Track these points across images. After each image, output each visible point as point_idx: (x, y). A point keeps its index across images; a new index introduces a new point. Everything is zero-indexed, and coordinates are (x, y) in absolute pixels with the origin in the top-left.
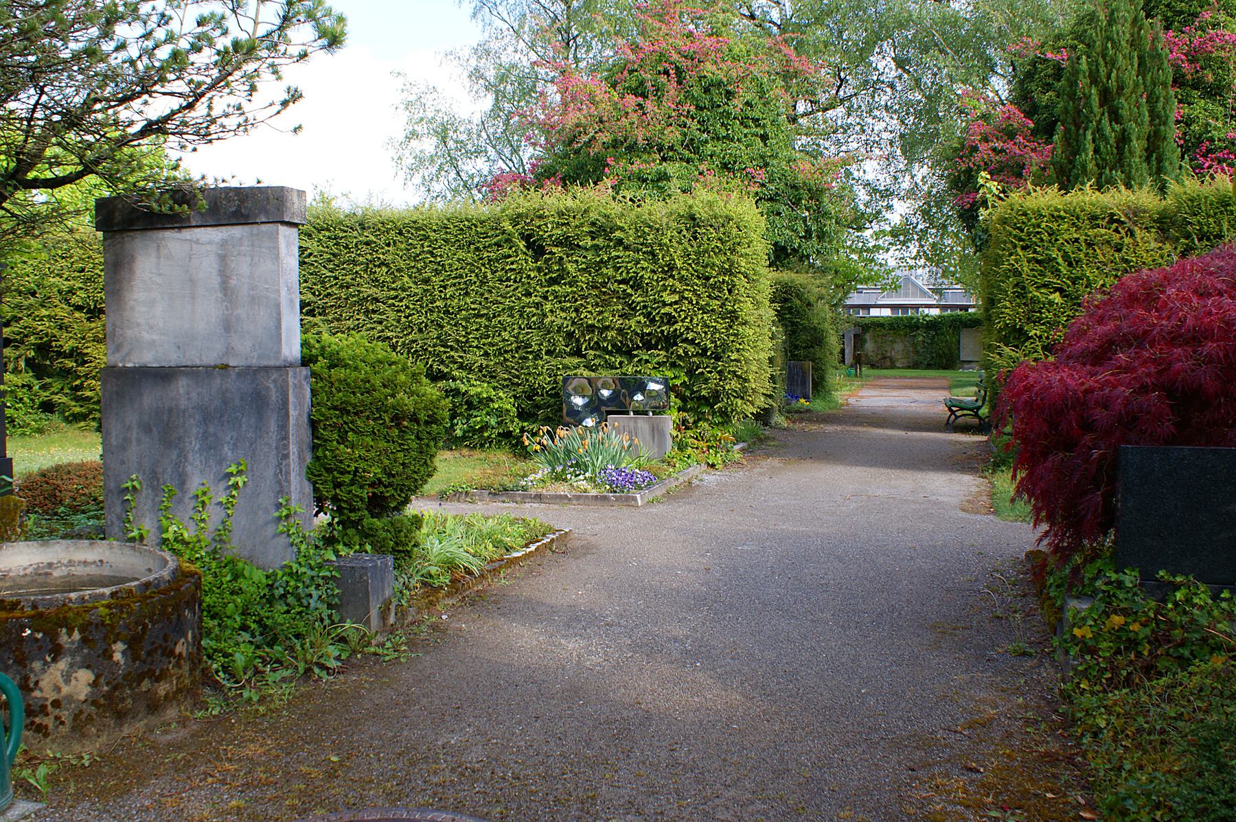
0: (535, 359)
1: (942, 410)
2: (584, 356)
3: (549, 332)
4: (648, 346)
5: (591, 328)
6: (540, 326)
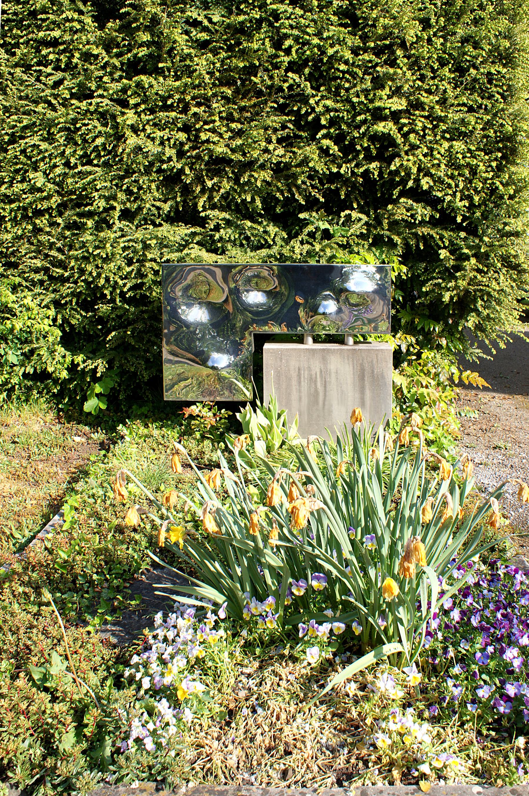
0: (98, 228)
1: (313, 373)
2: (202, 222)
3: (129, 172)
4: (333, 206)
5: (217, 165)
6: (110, 158)
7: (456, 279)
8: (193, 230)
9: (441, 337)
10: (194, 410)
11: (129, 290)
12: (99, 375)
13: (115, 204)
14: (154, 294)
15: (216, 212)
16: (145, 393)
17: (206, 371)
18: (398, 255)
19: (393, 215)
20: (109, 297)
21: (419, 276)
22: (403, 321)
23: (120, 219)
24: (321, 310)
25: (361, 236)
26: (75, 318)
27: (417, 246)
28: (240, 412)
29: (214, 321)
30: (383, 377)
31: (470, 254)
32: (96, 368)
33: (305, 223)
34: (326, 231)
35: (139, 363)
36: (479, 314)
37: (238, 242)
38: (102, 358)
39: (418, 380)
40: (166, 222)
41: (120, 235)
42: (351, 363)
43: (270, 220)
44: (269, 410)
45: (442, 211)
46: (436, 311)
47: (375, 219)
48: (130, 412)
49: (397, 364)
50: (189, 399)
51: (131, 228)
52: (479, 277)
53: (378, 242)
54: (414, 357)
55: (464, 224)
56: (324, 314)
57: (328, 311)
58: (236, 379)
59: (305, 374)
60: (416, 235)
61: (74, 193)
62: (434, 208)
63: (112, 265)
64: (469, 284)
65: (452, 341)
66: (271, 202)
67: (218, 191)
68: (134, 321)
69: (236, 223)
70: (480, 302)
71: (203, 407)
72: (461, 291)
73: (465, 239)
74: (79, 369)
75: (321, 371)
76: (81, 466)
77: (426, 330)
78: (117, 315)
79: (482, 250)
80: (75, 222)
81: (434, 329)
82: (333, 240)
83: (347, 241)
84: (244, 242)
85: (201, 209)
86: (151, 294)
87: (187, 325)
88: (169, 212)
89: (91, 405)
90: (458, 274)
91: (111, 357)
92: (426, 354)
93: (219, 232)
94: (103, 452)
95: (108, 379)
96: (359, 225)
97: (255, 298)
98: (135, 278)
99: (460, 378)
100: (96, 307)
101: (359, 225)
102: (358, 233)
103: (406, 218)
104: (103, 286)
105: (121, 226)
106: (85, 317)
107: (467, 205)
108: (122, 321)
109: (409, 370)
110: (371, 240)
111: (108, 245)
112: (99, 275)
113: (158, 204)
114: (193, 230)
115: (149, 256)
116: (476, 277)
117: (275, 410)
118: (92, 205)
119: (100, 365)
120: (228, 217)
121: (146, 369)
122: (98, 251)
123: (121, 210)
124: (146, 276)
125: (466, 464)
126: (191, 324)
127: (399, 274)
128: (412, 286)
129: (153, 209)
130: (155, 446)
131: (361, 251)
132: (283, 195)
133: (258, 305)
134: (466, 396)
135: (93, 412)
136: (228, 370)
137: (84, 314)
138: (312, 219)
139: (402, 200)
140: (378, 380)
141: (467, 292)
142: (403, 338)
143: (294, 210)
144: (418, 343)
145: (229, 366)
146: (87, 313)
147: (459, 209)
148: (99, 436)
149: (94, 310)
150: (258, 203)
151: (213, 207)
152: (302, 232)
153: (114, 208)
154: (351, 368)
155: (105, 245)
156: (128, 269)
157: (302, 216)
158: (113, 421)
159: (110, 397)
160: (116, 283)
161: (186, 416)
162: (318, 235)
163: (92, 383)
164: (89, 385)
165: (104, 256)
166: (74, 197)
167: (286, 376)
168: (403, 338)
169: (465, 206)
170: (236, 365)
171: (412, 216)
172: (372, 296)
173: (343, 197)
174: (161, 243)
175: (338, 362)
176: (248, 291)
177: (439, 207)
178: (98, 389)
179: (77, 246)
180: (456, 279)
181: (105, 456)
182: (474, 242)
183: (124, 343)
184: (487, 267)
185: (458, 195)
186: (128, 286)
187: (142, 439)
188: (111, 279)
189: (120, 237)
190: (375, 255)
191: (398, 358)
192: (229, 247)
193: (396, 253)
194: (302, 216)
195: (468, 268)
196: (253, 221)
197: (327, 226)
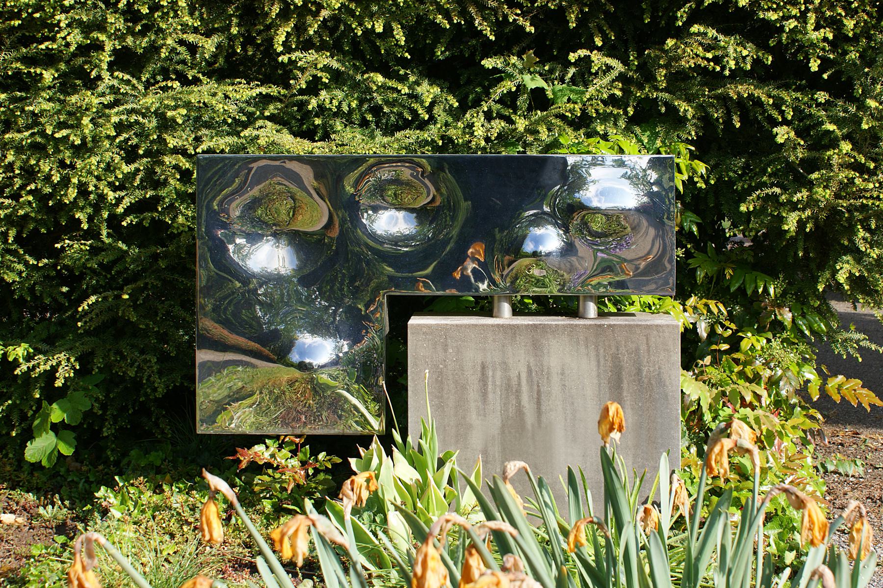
0: (65, 86)
1: (513, 374)
2: (282, 75)
7: (810, 185)
8: (264, 90)
9: (780, 306)
10: (261, 452)
11: (128, 211)
12: (59, 383)
13: (103, 37)
14: (181, 219)
15: (312, 56)
16: (156, 424)
17: (285, 374)
18: (687, 141)
19: (678, 58)
20: (85, 226)
21: (731, 182)
22: (700, 275)
23: (111, 67)
24: (529, 247)
25: (612, 100)
26: (12, 270)
27: (728, 122)
28: (358, 456)
29: (306, 271)
30: (661, 382)
31: (839, 133)
32: (54, 369)
33: (496, 76)
34: (538, 93)
35: (146, 361)
36: (859, 256)
37: (356, 117)
38: (70, 350)
39: (733, 391)
40: (209, 75)
41: (109, 103)
42: (593, 354)
43: (423, 75)
44: (421, 450)
45: (778, 51)
46: (771, 253)
47: (639, 68)
48: (125, 461)
49: (687, 364)
50: (247, 430)
51: (134, 88)
52: (858, 181)
53: (646, 117)
54: (725, 347)
55: (825, 76)
56: (535, 254)
57: (544, 249)
58: (348, 391)
59: (496, 377)
60: (724, 99)
61: (18, 16)
62: (762, 45)
63: (94, 160)
64: (837, 196)
65: (803, 315)
66: (425, 38)
67: (316, 14)
68: (135, 277)
69: (352, 78)
70: (862, 233)
71: (280, 447)
72: (822, 210)
73: (826, 106)
74: (17, 372)
75: (530, 371)
76: (12, 570)
77: (749, 292)
78: (101, 265)
79: (865, 126)
80: (18, 73)
81: (766, 290)
82: (553, 110)
83: (583, 111)
84: (369, 117)
85: (280, 49)
86: (174, 219)
87: (245, 277)
88: (215, 56)
89: (40, 448)
90: (815, 176)
91: (88, 348)
92: (750, 341)
93: (317, 95)
94: (61, 539)
95: (80, 394)
96: (607, 80)
97: (390, 223)
98: (141, 187)
99: (822, 389)
100: (58, 246)
101: (607, 80)
102: (605, 96)
103: (704, 63)
104: (74, 202)
105: (115, 83)
106: (35, 267)
107: (830, 36)
108: (112, 275)
109: (714, 373)
110: (631, 111)
111: (86, 121)
112: (65, 182)
113: (191, 38)
114: (264, 90)
115: (172, 142)
116: (851, 181)
117: (433, 450)
118: (53, 39)
119: (63, 365)
120: (335, 65)
121: (160, 373)
122: (64, 132)
123: (115, 51)
124: (165, 183)
125: (858, 525)
126: (254, 276)
127: (691, 179)
128: (718, 205)
129: (181, 49)
130: (174, 526)
131: (612, 131)
132: (450, 21)
133: (396, 240)
134: (834, 435)
135: (45, 463)
136: (334, 371)
137: (32, 261)
138: (509, 70)
139: (695, 28)
140: (649, 390)
141: (833, 212)
142: (700, 306)
143: (473, 55)
144: (731, 317)
145: (335, 363)
146: (38, 259)
147: (813, 45)
148: (54, 511)
149: (57, 254)
150: (400, 36)
151: (306, 45)
152: (488, 94)
153: (100, 47)
154: (594, 363)
155: (79, 120)
156: (126, 169)
157: (488, 63)
158: (87, 481)
159: (83, 432)
160: (102, 197)
161: (244, 465)
162: (522, 101)
163: (45, 403)
164: (39, 407)
165: (78, 142)
166: (17, 23)
167: (456, 382)
168: (700, 306)
169: (825, 39)
170: (351, 362)
171: (717, 60)
172: (635, 217)
173: (573, 25)
174: (198, 119)
175: (567, 354)
176: (376, 209)
177: (772, 43)
178: (57, 414)
179: (21, 121)
180: (810, 185)
181: (64, 546)
182: (846, 111)
183: (114, 321)
184: (874, 160)
185: (812, 17)
186: (126, 202)
187: (149, 514)
188: (91, 188)
189: (110, 106)
190: (640, 141)
191: (692, 348)
192: (339, 126)
193: (684, 136)
194: (488, 63)
195: (835, 160)
196: (387, 75)
197: (540, 83)
